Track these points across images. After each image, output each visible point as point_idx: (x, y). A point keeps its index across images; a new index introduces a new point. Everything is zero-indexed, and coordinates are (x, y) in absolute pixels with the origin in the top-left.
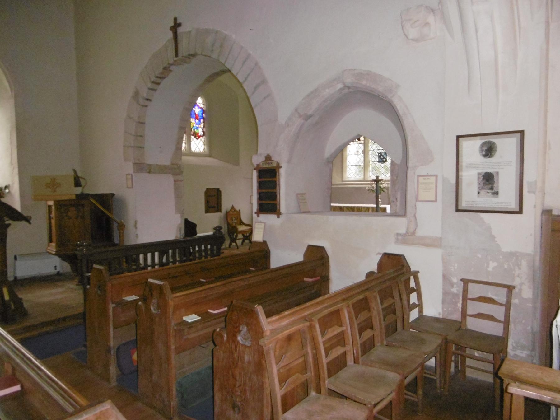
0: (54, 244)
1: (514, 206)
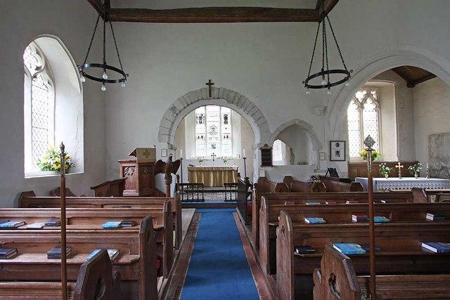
0: (229, 126)
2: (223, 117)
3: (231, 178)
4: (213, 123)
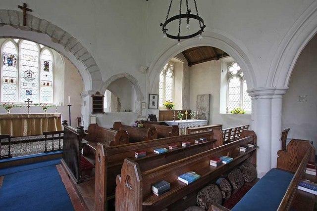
0: (50, 73)
2: (43, 63)
3: (51, 125)
4: (29, 68)
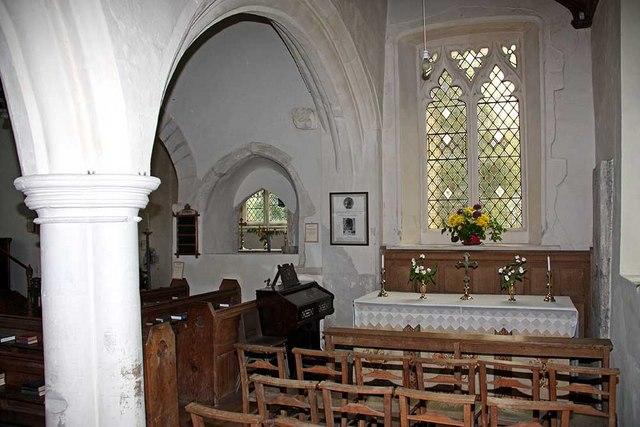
1: (364, 241)
